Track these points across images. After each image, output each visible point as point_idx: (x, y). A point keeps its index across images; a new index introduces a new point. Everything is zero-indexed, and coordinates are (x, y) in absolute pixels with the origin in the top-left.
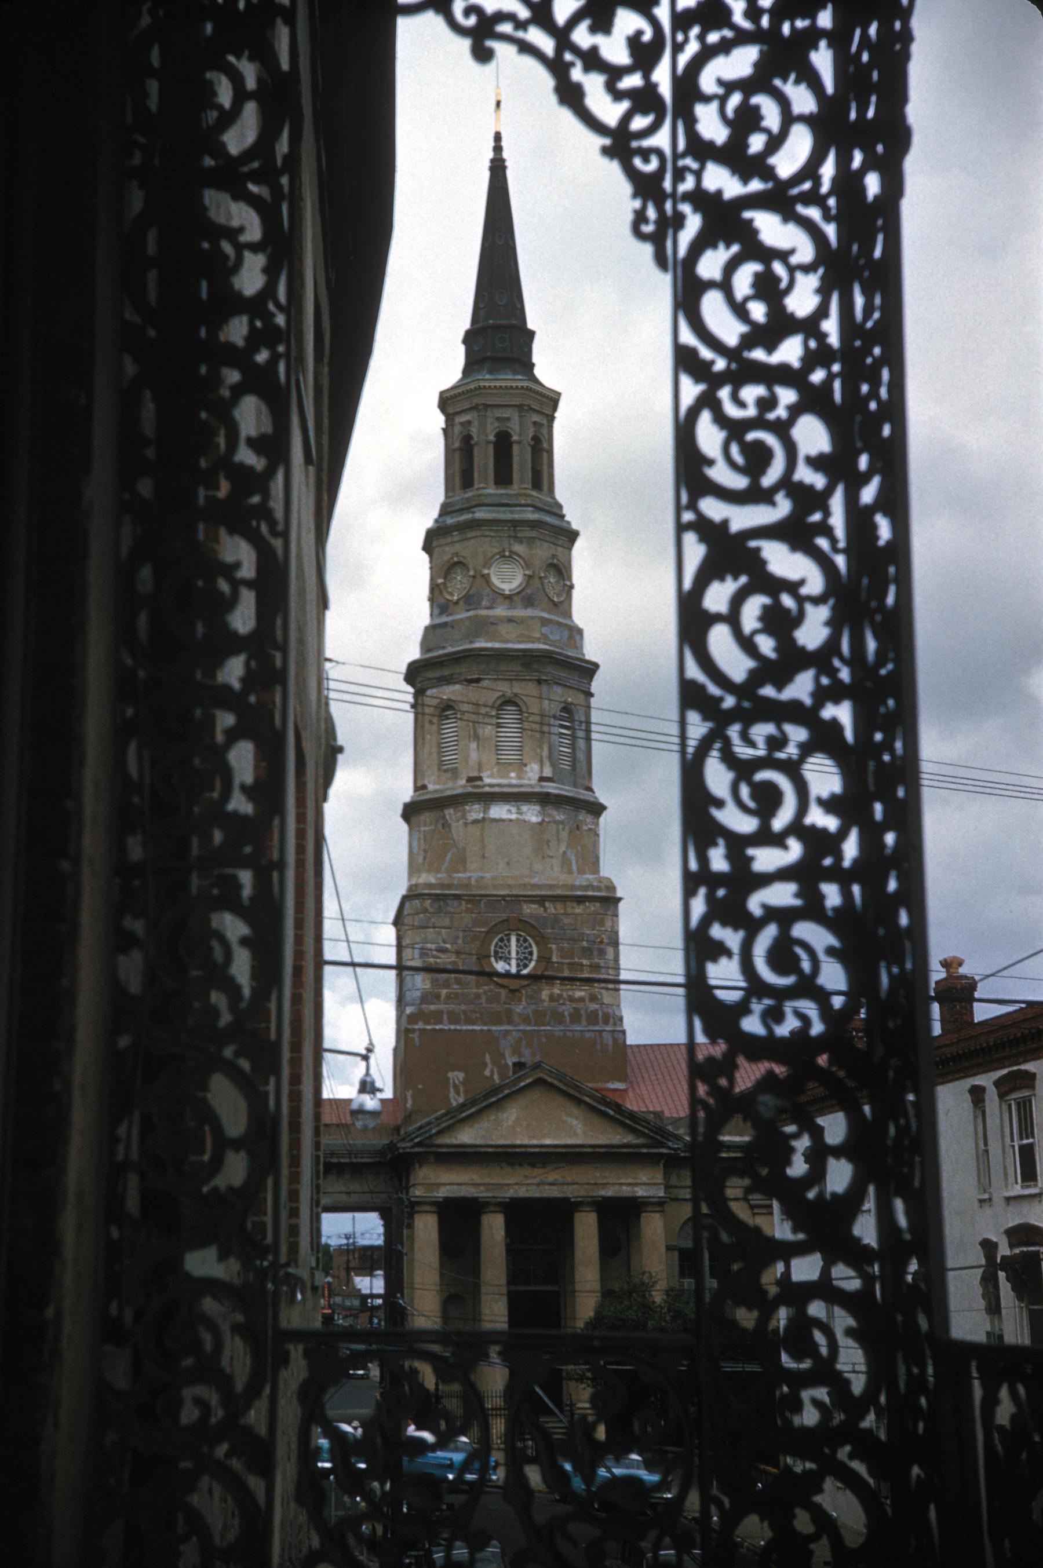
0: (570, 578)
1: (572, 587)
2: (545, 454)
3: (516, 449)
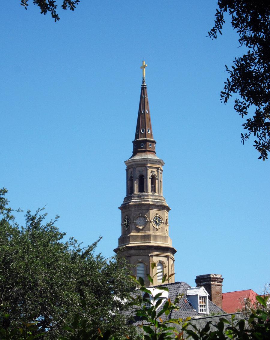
3: (157, 181)
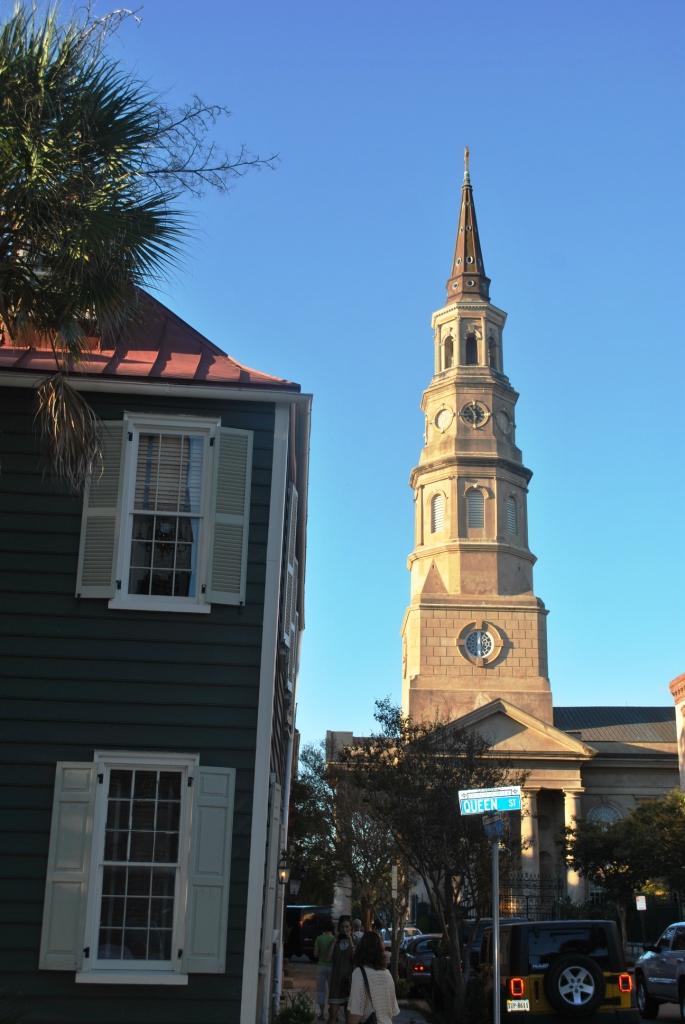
0: (513, 421)
1: (514, 426)
2: (497, 349)
